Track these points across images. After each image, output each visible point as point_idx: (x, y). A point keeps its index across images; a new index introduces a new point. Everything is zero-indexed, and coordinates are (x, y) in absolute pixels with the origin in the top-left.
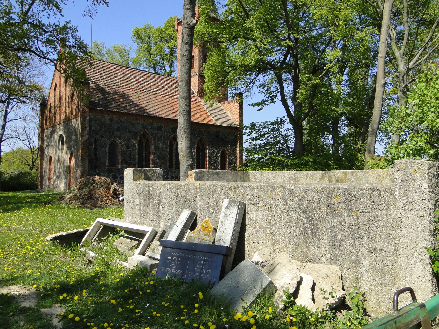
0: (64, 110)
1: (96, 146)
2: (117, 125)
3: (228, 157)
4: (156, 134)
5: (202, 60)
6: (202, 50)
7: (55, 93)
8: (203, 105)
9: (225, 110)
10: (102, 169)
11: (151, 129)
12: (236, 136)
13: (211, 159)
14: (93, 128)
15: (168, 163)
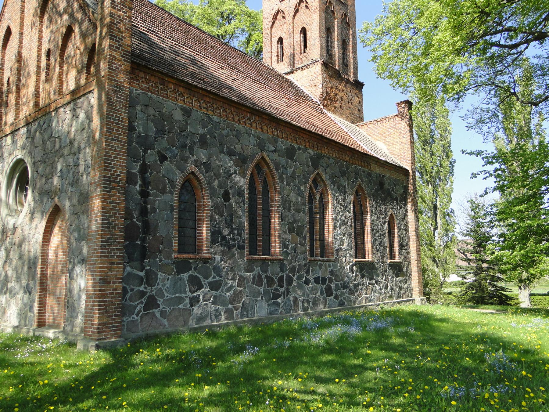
0: (31, 89)
1: (145, 183)
2: (201, 131)
6: (323, 15)
10: (161, 260)
11: (275, 151)
12: (406, 188)
15: (308, 243)
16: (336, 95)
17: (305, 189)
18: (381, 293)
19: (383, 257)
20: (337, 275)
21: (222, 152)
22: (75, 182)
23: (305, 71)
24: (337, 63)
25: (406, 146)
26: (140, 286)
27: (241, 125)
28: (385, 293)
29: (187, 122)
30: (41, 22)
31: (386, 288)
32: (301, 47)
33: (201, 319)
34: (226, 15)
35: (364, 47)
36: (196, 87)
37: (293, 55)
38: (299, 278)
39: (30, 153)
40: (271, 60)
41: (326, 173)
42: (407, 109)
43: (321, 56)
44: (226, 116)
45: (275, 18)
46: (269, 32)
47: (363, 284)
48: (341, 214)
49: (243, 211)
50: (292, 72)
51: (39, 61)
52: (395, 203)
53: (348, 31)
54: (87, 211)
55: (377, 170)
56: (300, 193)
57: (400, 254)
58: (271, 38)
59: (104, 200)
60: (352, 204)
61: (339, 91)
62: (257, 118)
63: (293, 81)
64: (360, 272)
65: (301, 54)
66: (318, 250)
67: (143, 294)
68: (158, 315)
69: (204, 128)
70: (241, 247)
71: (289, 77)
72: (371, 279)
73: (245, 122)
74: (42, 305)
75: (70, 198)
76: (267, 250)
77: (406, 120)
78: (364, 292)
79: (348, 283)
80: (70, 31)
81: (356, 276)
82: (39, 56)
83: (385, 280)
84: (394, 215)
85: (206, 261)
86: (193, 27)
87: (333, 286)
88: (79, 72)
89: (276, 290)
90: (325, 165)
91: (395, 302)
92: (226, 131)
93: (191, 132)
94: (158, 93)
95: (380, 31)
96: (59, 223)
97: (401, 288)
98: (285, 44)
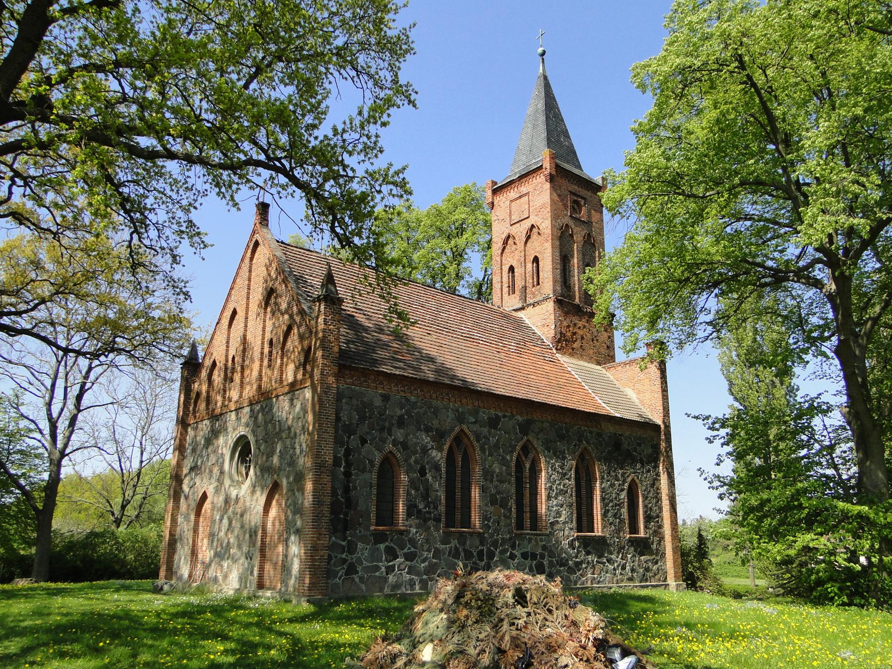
0: (255, 373)
1: (348, 465)
2: (399, 412)
3: (643, 501)
4: (485, 437)
5: (559, 266)
6: (558, 243)
7: (229, 334)
8: (569, 369)
9: (616, 382)
10: (360, 532)
11: (475, 422)
12: (656, 447)
13: (607, 505)
14: (344, 418)
15: (514, 515)
16: (574, 334)
17: (512, 459)
18: (615, 574)
19: (618, 531)
20: (551, 551)
21: (419, 429)
22: (292, 463)
25: (656, 395)
26: (343, 553)
28: (621, 574)
30: (265, 313)
31: (624, 568)
33: (396, 586)
38: (503, 552)
39: (253, 431)
41: (538, 439)
43: (554, 291)
45: (506, 242)
46: (498, 259)
47: (588, 563)
48: (557, 482)
49: (440, 484)
50: (522, 308)
51: (262, 348)
52: (638, 466)
53: (594, 252)
54: (302, 489)
55: (611, 429)
56: (504, 462)
57: (646, 527)
59: (316, 482)
60: (573, 472)
64: (585, 548)
66: (527, 523)
67: (344, 561)
68: (357, 580)
70: (438, 520)
72: (599, 557)
74: (262, 569)
75: (288, 477)
76: (467, 522)
78: (590, 571)
79: (567, 560)
80: (290, 328)
81: (578, 552)
82: (263, 343)
83: (622, 559)
84: (637, 481)
85: (401, 533)
87: (546, 562)
88: (297, 368)
89: (475, 563)
90: (537, 430)
91: (636, 586)
94: (360, 385)
96: (277, 497)
97: (647, 570)
98: (516, 274)
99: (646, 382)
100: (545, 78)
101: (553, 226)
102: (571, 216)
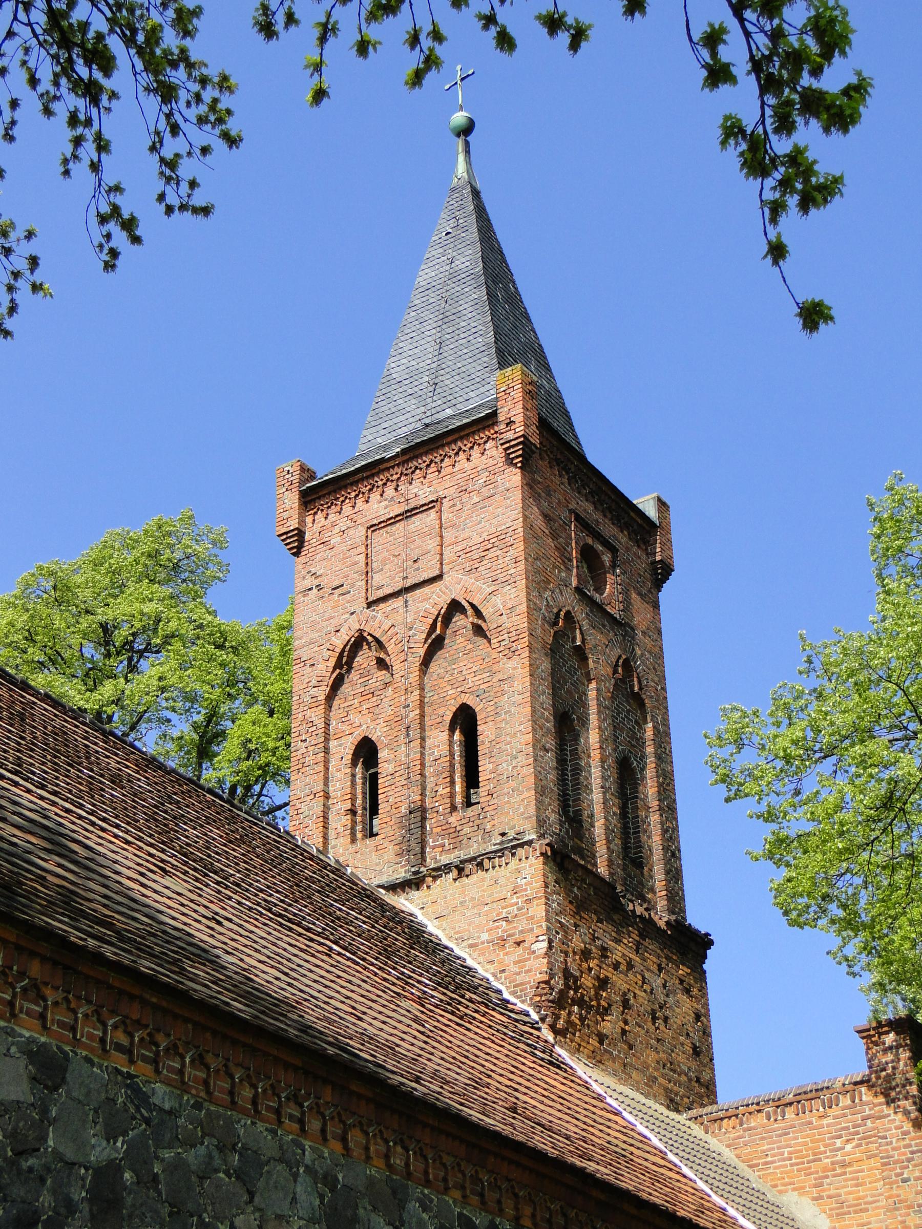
6: (545, 665)
9: (747, 1172)
16: (603, 983)
23: (474, 878)
24: (601, 849)
27: (261, 1126)
29: (45, 1111)
32: (452, 783)
34: (120, 636)
35: (728, 800)
36: (98, 957)
37: (420, 813)
40: (325, 827)
42: (905, 1055)
43: (541, 822)
44: (206, 1083)
46: (317, 716)
50: (414, 883)
53: (640, 724)
58: (327, 740)
61: (616, 966)
62: (328, 1094)
63: (421, 917)
65: (453, 808)
69: (110, 1137)
71: (405, 903)
73: (278, 1112)
77: (908, 1104)
86: (36, 694)
92: (202, 1150)
93: (58, 1155)
95: (795, 743)
98: (385, 768)
99: (870, 1169)
100: (476, 193)
101: (532, 609)
102: (578, 590)
